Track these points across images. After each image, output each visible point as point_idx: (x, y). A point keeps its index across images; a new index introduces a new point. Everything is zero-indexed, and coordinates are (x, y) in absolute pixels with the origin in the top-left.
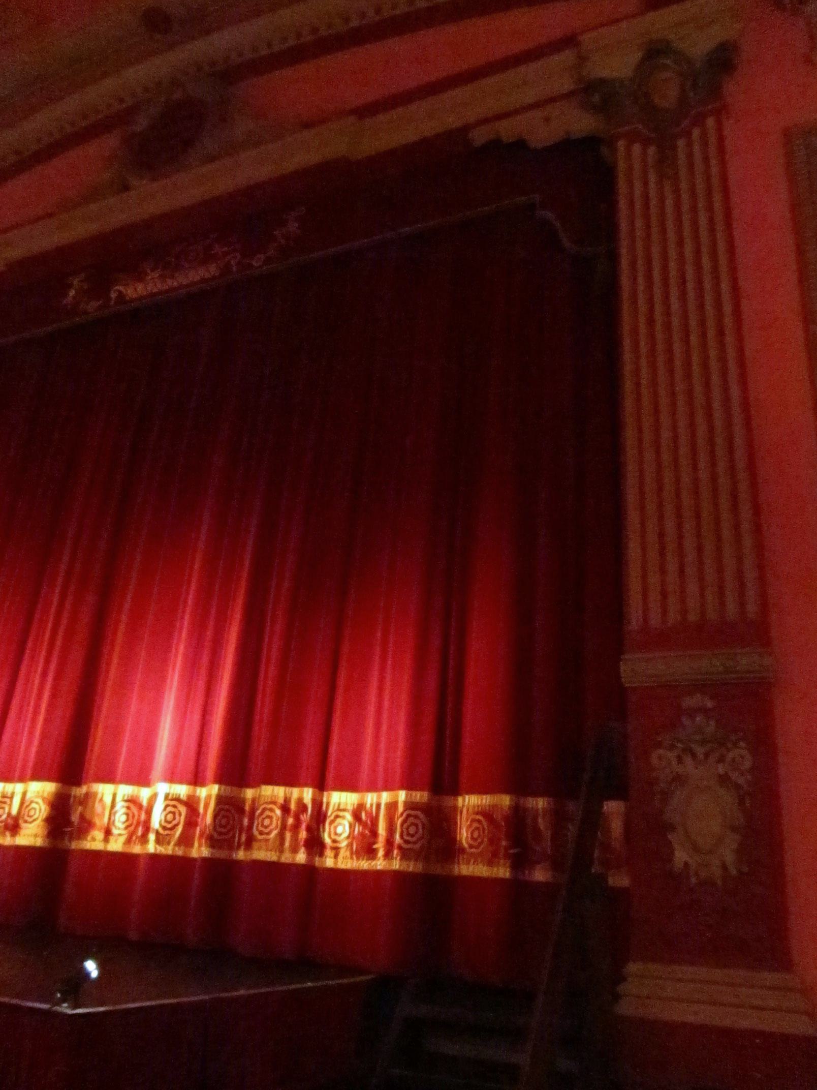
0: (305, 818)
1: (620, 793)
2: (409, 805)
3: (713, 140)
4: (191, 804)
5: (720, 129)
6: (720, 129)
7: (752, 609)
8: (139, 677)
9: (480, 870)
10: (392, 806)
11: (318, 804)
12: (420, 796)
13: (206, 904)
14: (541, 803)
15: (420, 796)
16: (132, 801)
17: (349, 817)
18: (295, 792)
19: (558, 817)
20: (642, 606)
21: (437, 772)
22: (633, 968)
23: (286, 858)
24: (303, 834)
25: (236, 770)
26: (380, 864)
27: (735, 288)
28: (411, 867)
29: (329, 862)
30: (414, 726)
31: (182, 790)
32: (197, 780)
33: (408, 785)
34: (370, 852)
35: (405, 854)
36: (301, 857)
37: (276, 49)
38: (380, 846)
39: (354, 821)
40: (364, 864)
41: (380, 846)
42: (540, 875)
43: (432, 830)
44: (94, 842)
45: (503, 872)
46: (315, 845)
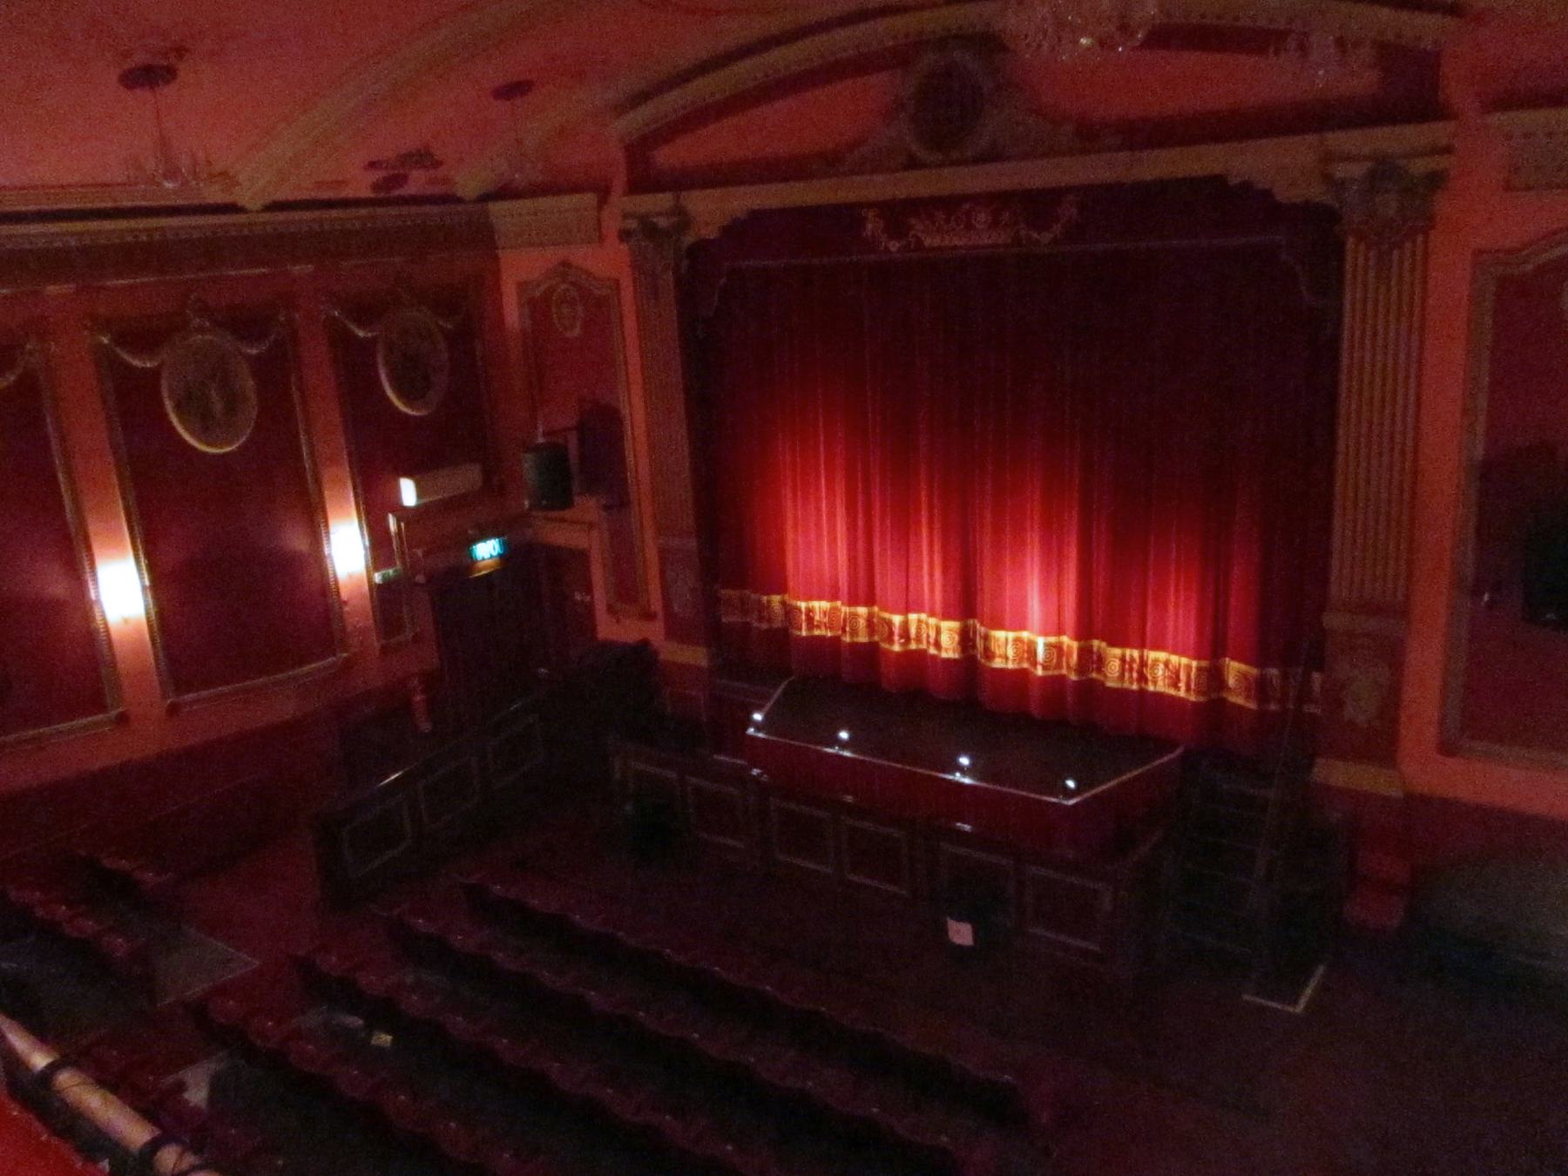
0: (1135, 666)
1: (1320, 669)
2: (1199, 669)
3: (1419, 252)
4: (1058, 647)
5: (1426, 242)
6: (1426, 242)
7: (1400, 597)
8: (1007, 560)
9: (1240, 701)
10: (1189, 667)
11: (1141, 657)
12: (1204, 663)
13: (1071, 718)
14: (1274, 671)
15: (1204, 663)
16: (1017, 640)
17: (1161, 666)
18: (1128, 652)
19: (1285, 676)
20: (1338, 589)
21: (1212, 649)
22: (1320, 761)
23: (1126, 685)
24: (1135, 675)
25: (1084, 632)
26: (1182, 693)
27: (1418, 398)
28: (1202, 699)
29: (1151, 688)
30: (1200, 632)
31: (1052, 639)
32: (1060, 631)
33: (1198, 657)
34: (1175, 685)
35: (1198, 692)
36: (1135, 687)
37: (1207, 21)
38: (1182, 685)
39: (1168, 669)
40: (1172, 692)
41: (1182, 685)
42: (1273, 707)
43: (1213, 678)
44: (998, 663)
45: (1252, 705)
46: (1142, 678)
